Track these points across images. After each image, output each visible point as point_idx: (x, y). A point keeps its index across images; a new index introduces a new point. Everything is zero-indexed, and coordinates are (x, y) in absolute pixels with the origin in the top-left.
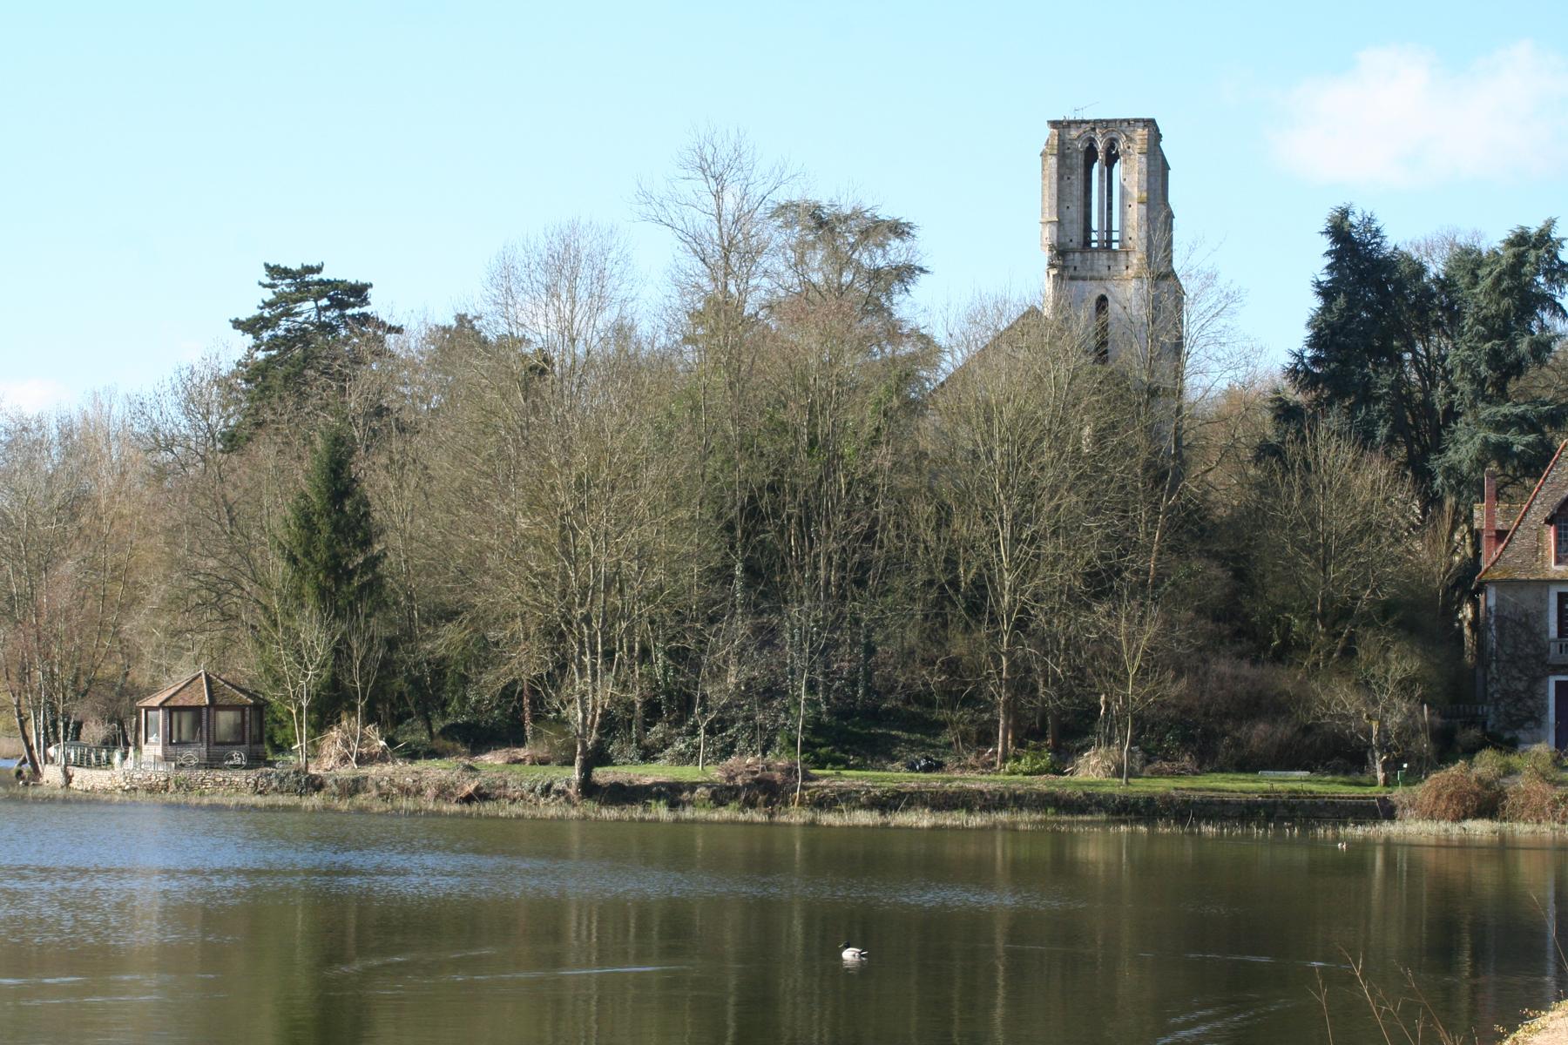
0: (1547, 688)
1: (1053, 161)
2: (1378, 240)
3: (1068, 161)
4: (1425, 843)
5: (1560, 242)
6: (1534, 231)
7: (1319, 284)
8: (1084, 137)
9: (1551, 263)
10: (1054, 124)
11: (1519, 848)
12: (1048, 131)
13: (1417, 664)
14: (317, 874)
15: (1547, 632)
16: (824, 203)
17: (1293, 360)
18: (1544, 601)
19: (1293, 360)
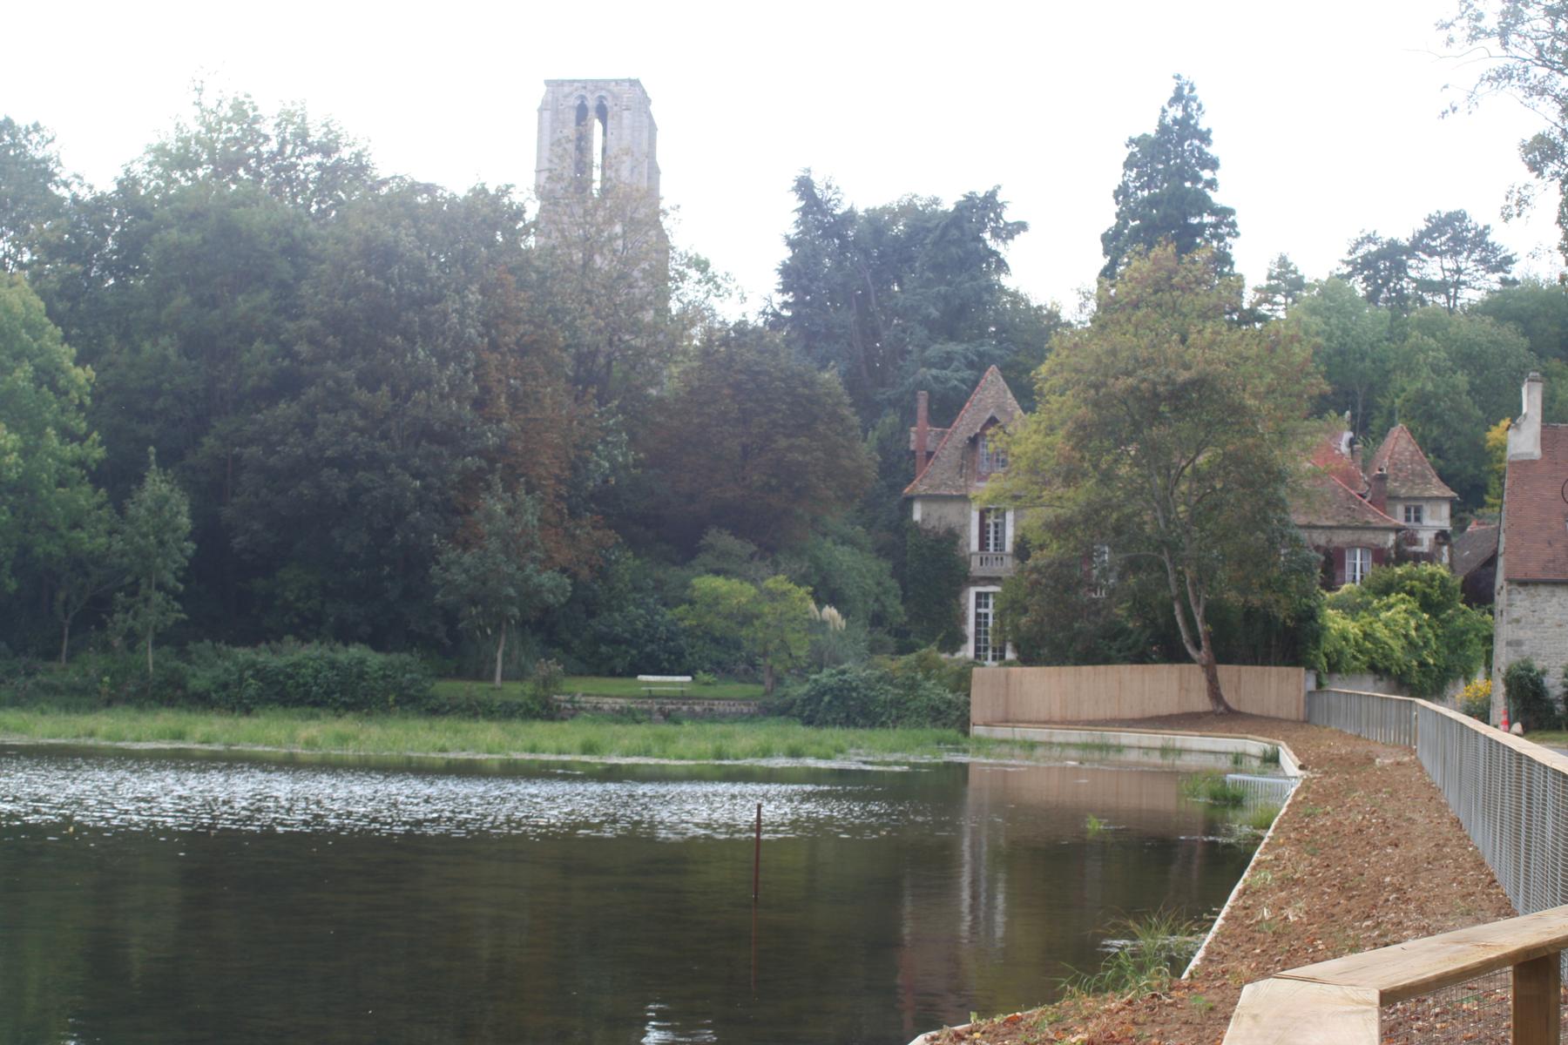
0: (968, 599)
1: (547, 115)
2: (838, 196)
3: (561, 117)
4: (1544, 592)
5: (1002, 206)
6: (981, 195)
7: (787, 237)
8: (576, 94)
9: (997, 221)
10: (548, 83)
11: (759, 819)
12: (544, 88)
13: (1489, 435)
14: (891, 683)
15: (968, 545)
16: (64, 174)
17: (765, 303)
18: (967, 516)
19: (765, 303)
